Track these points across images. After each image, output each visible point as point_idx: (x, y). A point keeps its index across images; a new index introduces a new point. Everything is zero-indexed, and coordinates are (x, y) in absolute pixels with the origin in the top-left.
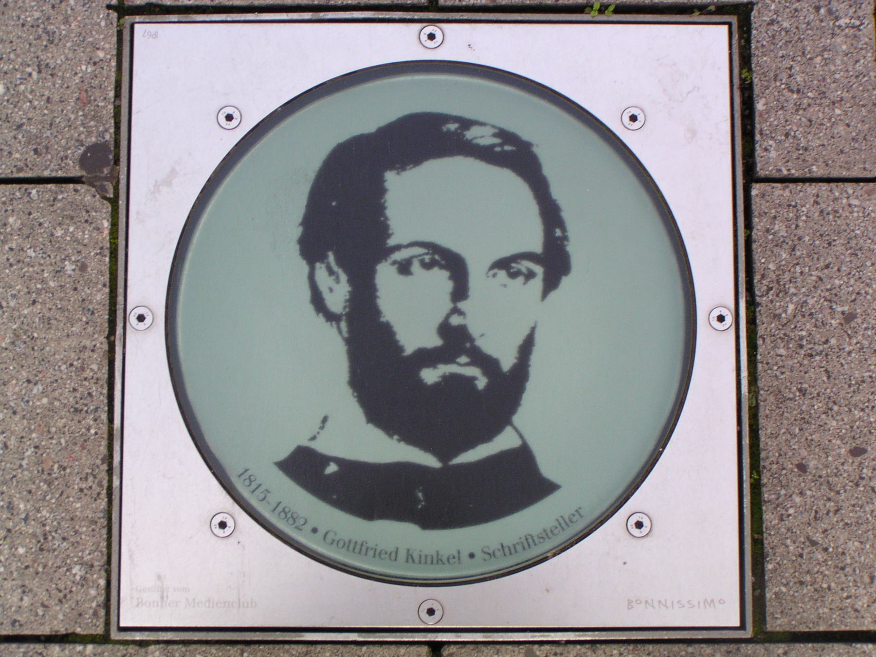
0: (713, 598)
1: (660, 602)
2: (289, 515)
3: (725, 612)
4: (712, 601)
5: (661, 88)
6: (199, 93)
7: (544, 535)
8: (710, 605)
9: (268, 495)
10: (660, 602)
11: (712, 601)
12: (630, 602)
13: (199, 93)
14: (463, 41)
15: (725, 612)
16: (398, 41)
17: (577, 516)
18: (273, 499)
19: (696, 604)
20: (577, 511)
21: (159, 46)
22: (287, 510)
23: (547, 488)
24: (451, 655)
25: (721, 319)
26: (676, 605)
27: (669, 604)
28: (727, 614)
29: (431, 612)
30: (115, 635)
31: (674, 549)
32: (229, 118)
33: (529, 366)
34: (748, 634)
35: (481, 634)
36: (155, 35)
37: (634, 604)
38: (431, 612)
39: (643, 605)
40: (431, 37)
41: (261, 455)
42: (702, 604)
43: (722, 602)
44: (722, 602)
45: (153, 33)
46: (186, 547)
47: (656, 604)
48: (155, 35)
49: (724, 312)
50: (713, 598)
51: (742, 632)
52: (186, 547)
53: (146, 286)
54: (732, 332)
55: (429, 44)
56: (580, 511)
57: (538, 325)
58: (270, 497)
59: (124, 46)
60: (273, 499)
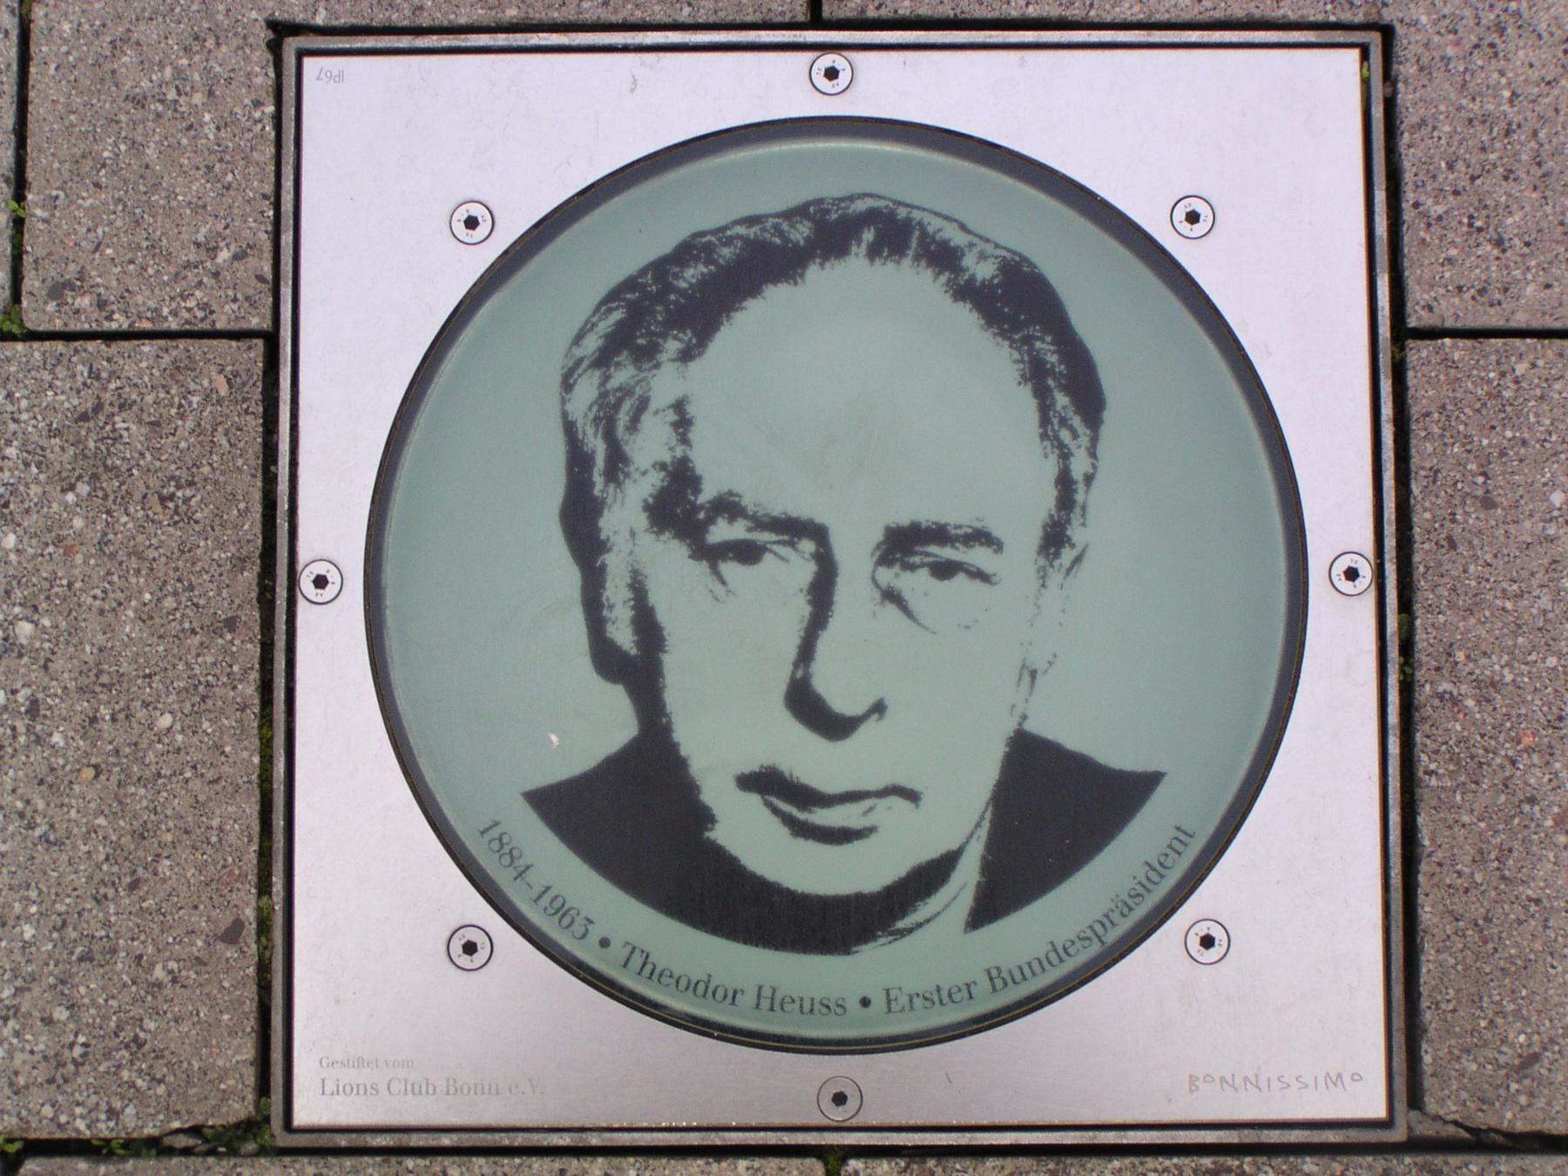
0: (1335, 1068)
1: (1246, 1079)
2: (506, 849)
4: (1340, 1076)
5: (1244, 171)
6: (420, 179)
7: (1140, 890)
8: (1335, 1084)
9: (590, 927)
10: (1246, 1079)
12: (1193, 1079)
13: (420, 179)
14: (892, 83)
16: (776, 84)
17: (965, 993)
19: (1311, 1083)
20: (968, 986)
22: (505, 840)
23: (1132, 790)
24: (856, 1173)
25: (1352, 574)
26: (1275, 1084)
28: (1367, 1099)
31: (1269, 976)
35: (1078, 1134)
36: (340, 78)
38: (840, 1099)
41: (497, 800)
42: (1321, 1081)
43: (1357, 1077)
44: (1357, 1077)
45: (335, 73)
49: (852, 1103)
50: (1335, 1068)
54: (1370, 601)
56: (973, 989)
57: (873, 838)
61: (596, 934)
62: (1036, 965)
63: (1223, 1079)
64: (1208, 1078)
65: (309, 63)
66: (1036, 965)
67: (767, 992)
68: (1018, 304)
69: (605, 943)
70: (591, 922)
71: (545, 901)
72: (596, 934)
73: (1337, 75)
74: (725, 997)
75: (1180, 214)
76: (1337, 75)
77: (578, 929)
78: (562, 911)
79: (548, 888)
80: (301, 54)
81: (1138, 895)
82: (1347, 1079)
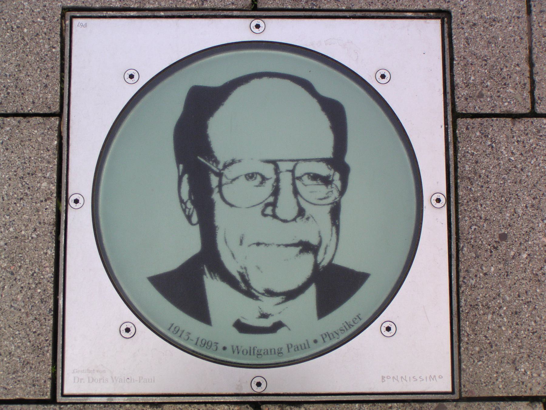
0: (436, 377)
1: (402, 377)
3: (444, 384)
4: (435, 376)
5: (402, 62)
6: (114, 60)
7: (344, 328)
9: (190, 336)
10: (402, 377)
11: (435, 376)
12: (383, 378)
13: (114, 60)
14: (277, 30)
15: (444, 384)
16: (237, 30)
18: (193, 337)
19: (425, 379)
21: (89, 35)
26: (412, 379)
27: (408, 379)
29: (259, 384)
30: (59, 399)
32: (131, 76)
33: (230, 94)
34: (456, 396)
36: (86, 26)
37: (386, 379)
39: (392, 379)
40: (258, 26)
42: (428, 379)
43: (441, 377)
44: (441, 377)
46: (106, 342)
47: (399, 379)
48: (86, 26)
51: (451, 396)
52: (106, 342)
53: (80, 181)
55: (256, 30)
58: (191, 337)
59: (425, 14)
60: (193, 337)
61: (220, 347)
62: (273, 351)
63: (394, 377)
64: (388, 377)
65: (76, 22)
66: (273, 351)
67: (174, 326)
68: (334, 112)
69: (225, 348)
70: (217, 343)
71: (172, 329)
72: (220, 347)
73: (434, 27)
74: (247, 353)
75: (378, 75)
76: (434, 27)
77: (184, 335)
78: (177, 330)
79: (172, 325)
80: (72, 17)
81: (344, 330)
82: (437, 377)
